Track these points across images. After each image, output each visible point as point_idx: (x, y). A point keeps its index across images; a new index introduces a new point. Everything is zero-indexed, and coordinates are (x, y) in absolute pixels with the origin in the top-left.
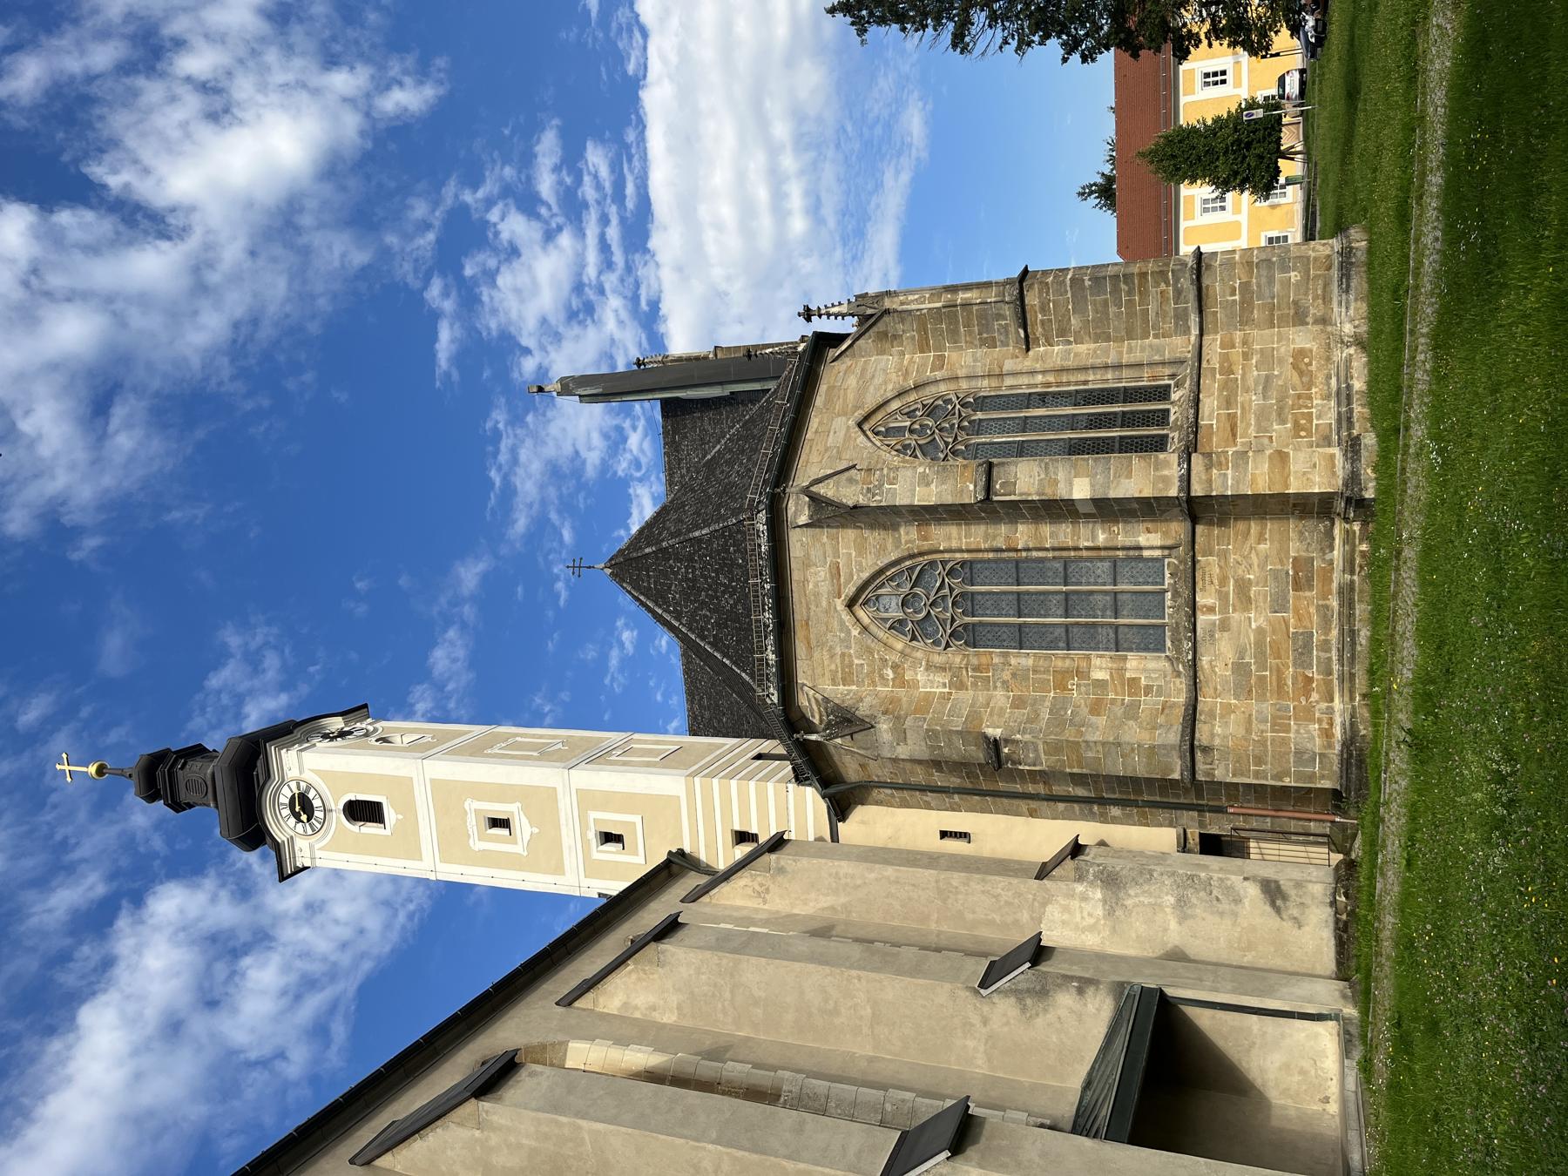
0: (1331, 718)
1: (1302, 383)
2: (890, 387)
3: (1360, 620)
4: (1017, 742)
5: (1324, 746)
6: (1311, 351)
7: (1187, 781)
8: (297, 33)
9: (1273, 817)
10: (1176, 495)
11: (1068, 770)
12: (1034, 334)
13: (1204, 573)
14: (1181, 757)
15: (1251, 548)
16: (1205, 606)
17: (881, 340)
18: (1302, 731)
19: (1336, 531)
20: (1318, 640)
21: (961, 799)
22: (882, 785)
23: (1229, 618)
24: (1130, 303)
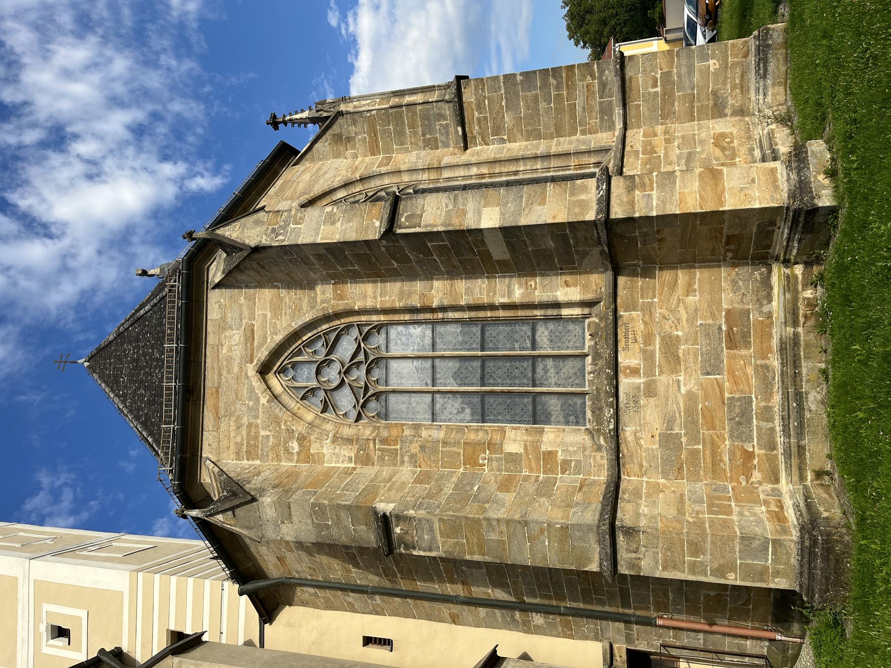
0: (780, 501)
1: (725, 155)
2: (339, 178)
3: (808, 381)
4: (410, 519)
5: (777, 531)
6: (732, 134)
7: (607, 574)
8: (147, 142)
9: (705, 632)
10: (593, 218)
11: (468, 557)
12: (472, 134)
13: (627, 330)
14: (599, 542)
15: (679, 300)
16: (629, 367)
17: (336, 144)
18: (746, 513)
19: (775, 279)
20: (758, 407)
21: (383, 601)
22: (304, 583)
23: (655, 381)
24: (558, 96)
